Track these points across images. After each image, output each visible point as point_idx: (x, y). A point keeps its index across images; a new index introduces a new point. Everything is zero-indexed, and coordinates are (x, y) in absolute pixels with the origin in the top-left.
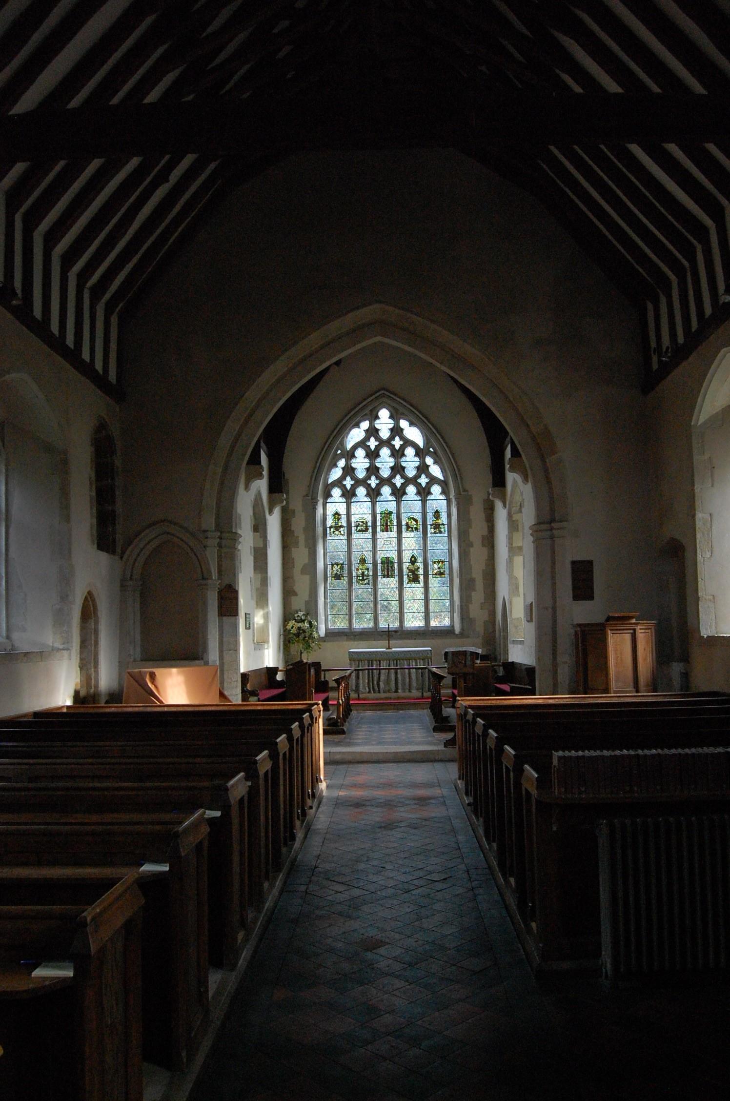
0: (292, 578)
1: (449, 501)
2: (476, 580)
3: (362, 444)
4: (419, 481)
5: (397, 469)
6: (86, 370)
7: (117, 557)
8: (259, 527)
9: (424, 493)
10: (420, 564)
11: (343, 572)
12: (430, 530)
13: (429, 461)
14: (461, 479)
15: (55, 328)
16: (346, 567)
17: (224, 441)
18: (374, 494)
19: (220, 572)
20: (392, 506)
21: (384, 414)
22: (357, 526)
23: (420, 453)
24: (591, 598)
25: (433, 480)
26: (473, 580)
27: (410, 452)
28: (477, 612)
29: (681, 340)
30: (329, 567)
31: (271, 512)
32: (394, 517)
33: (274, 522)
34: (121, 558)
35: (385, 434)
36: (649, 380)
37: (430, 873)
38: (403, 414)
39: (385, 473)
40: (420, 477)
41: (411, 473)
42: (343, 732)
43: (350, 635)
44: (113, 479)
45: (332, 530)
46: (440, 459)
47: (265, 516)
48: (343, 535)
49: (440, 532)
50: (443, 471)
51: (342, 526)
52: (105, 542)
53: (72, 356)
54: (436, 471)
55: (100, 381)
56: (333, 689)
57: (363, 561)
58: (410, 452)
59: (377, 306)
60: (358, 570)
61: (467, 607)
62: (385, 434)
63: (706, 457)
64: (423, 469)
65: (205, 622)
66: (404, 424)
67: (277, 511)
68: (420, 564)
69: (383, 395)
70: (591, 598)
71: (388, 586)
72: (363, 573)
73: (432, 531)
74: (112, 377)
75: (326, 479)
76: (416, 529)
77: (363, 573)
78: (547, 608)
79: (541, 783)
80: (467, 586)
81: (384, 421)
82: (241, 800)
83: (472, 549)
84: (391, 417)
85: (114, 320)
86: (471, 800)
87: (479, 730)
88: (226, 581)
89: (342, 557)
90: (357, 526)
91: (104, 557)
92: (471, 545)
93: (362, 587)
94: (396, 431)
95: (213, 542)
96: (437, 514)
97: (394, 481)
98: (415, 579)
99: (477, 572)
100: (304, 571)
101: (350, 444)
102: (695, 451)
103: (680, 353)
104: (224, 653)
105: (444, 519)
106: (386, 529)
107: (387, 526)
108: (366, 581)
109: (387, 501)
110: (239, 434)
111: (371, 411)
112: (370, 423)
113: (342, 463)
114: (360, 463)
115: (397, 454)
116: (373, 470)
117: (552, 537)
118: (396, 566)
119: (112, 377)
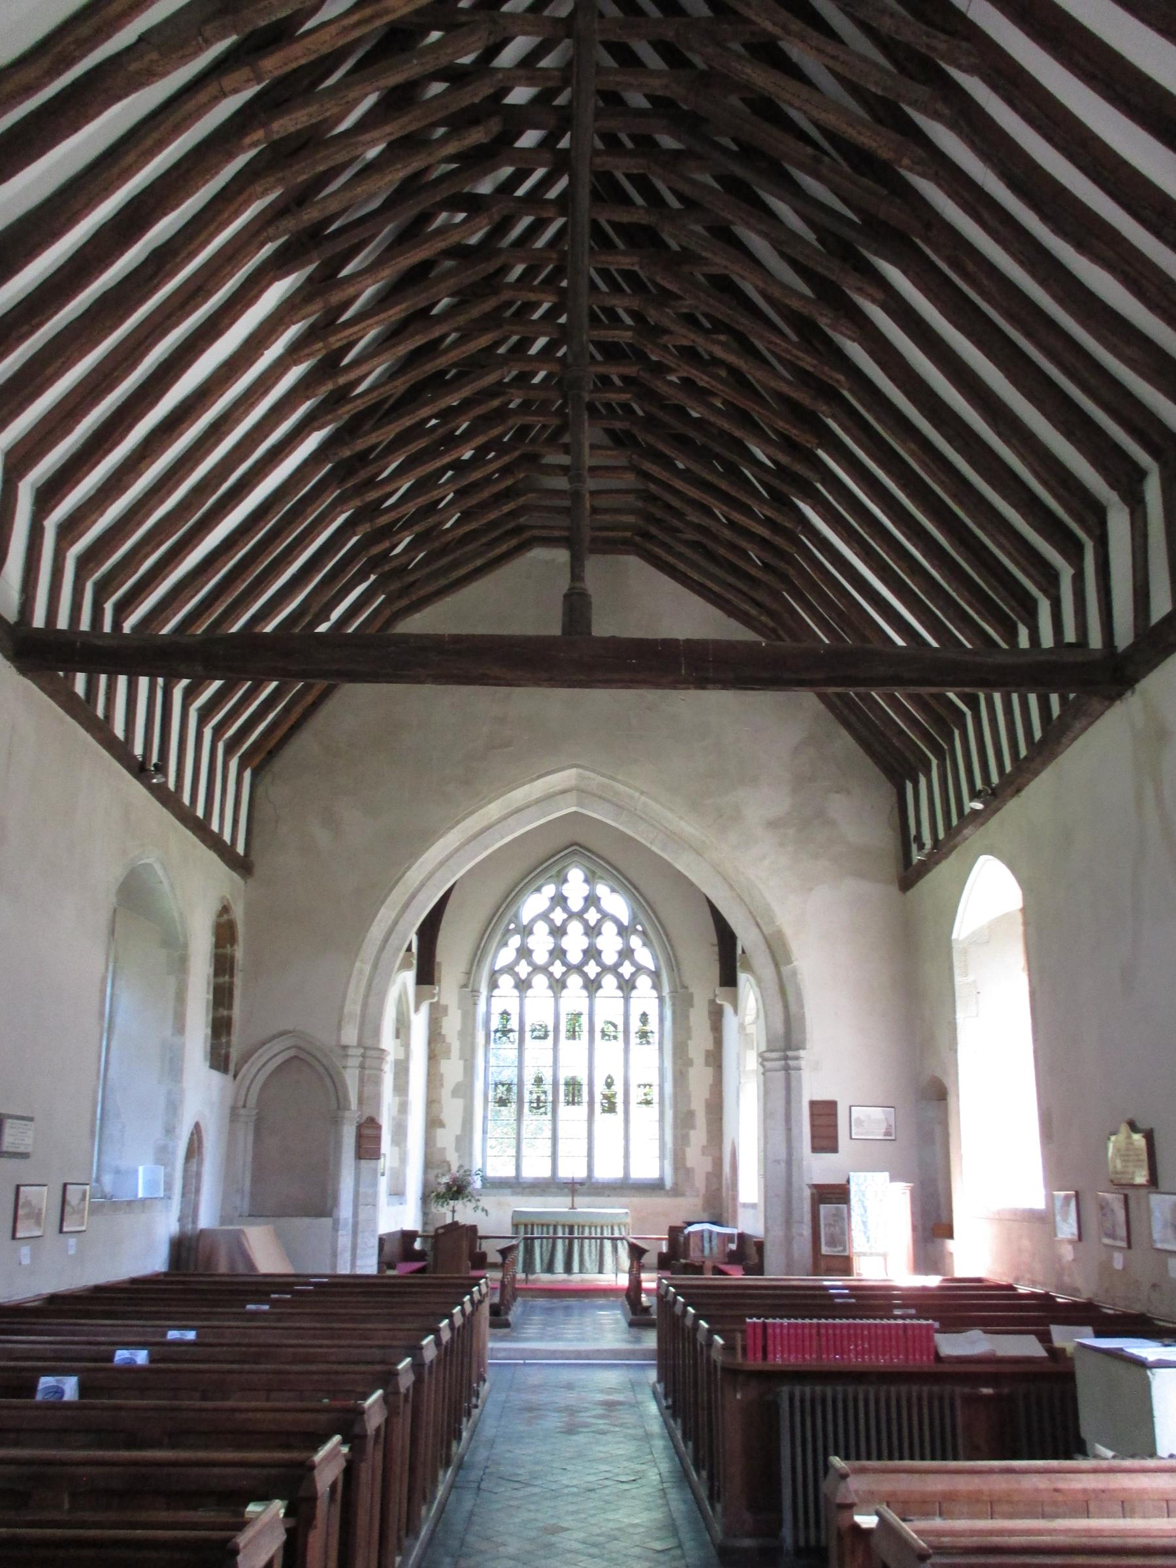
0: (439, 1102)
1: (661, 999)
2: (698, 1114)
3: (545, 916)
4: (620, 970)
5: (592, 953)
6: (213, 842)
7: (230, 1077)
8: (402, 1029)
9: (627, 986)
10: (618, 1088)
11: (507, 1096)
12: (634, 1039)
13: (635, 942)
14: (679, 970)
15: (186, 799)
16: (515, 1089)
17: (377, 931)
18: (558, 986)
19: (361, 1101)
20: (582, 1005)
21: (576, 875)
22: (533, 1031)
23: (623, 931)
24: (834, 1149)
25: (639, 969)
26: (691, 1114)
27: (609, 928)
28: (696, 1159)
29: (995, 779)
30: (491, 1087)
31: (417, 1009)
32: (584, 1020)
33: (419, 1023)
34: (235, 1076)
35: (576, 904)
36: (909, 875)
37: (618, 1475)
38: (601, 878)
39: (575, 957)
40: (621, 964)
41: (610, 958)
42: (507, 1325)
43: (516, 1185)
44: (232, 976)
45: (499, 1034)
46: (651, 942)
47: (409, 1016)
48: (513, 1043)
49: (648, 1043)
50: (655, 958)
51: (511, 1031)
52: (219, 1060)
53: (200, 828)
54: (644, 956)
55: (224, 851)
56: (494, 1266)
57: (539, 1081)
58: (609, 928)
59: (574, 771)
60: (531, 1093)
61: (684, 1152)
62: (576, 904)
63: (971, 978)
64: (626, 953)
65: (338, 1164)
66: (602, 890)
67: (425, 1008)
68: (618, 1088)
69: (574, 853)
70: (834, 1149)
71: (572, 1117)
72: (538, 1097)
73: (638, 1041)
74: (240, 849)
75: (493, 963)
76: (615, 1038)
77: (538, 1099)
78: (778, 1162)
79: (729, 1348)
80: (683, 1121)
81: (576, 885)
82: (432, 1362)
83: (690, 1069)
84: (586, 881)
85: (247, 774)
86: (670, 1401)
87: (678, 1309)
88: (368, 1112)
89: (510, 1075)
90: (533, 1031)
91: (216, 1076)
92: (690, 1063)
93: (538, 1117)
94: (592, 900)
95: (353, 1062)
96: (644, 1018)
97: (586, 969)
98: (611, 1108)
99: (698, 1105)
100: (455, 1093)
101: (525, 918)
102: (957, 971)
103: (941, 850)
104: (361, 1208)
105: (653, 1025)
106: (573, 1034)
107: (574, 1032)
108: (543, 1110)
109: (574, 996)
110: (396, 923)
111: (559, 872)
112: (557, 889)
113: (515, 941)
114: (541, 942)
115: (592, 931)
116: (558, 953)
117: (787, 1069)
118: (585, 1089)
119: (240, 849)
